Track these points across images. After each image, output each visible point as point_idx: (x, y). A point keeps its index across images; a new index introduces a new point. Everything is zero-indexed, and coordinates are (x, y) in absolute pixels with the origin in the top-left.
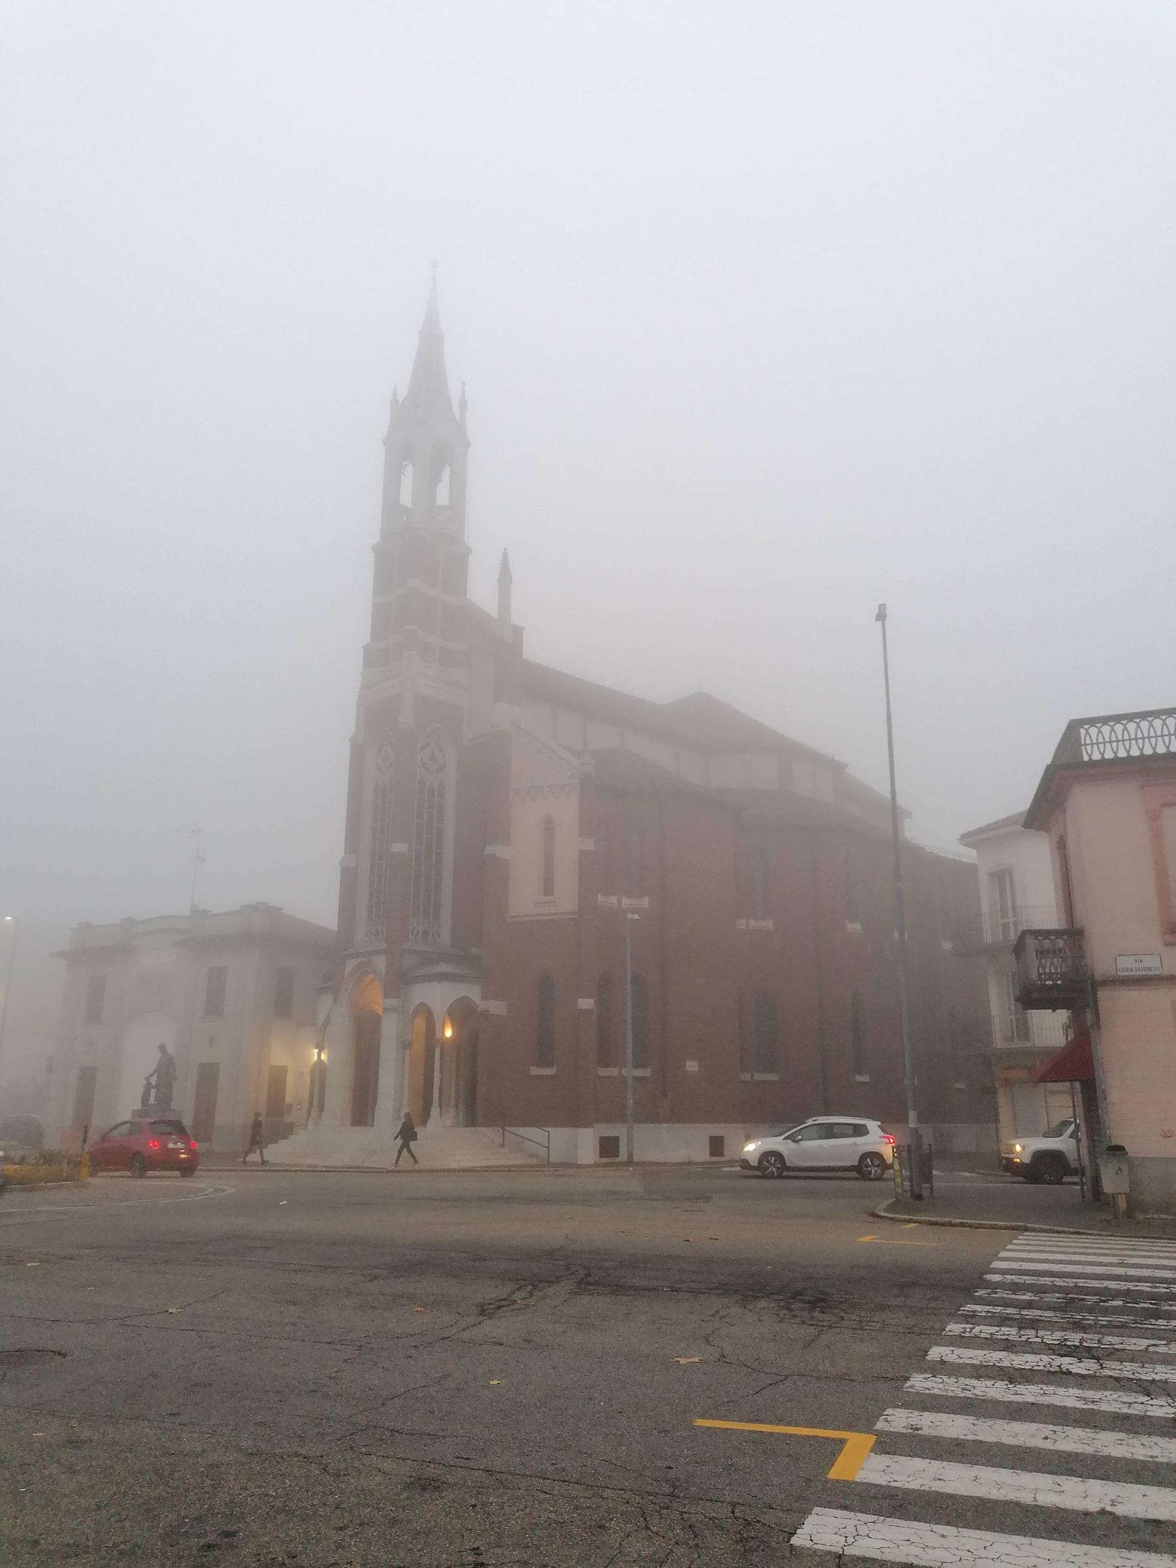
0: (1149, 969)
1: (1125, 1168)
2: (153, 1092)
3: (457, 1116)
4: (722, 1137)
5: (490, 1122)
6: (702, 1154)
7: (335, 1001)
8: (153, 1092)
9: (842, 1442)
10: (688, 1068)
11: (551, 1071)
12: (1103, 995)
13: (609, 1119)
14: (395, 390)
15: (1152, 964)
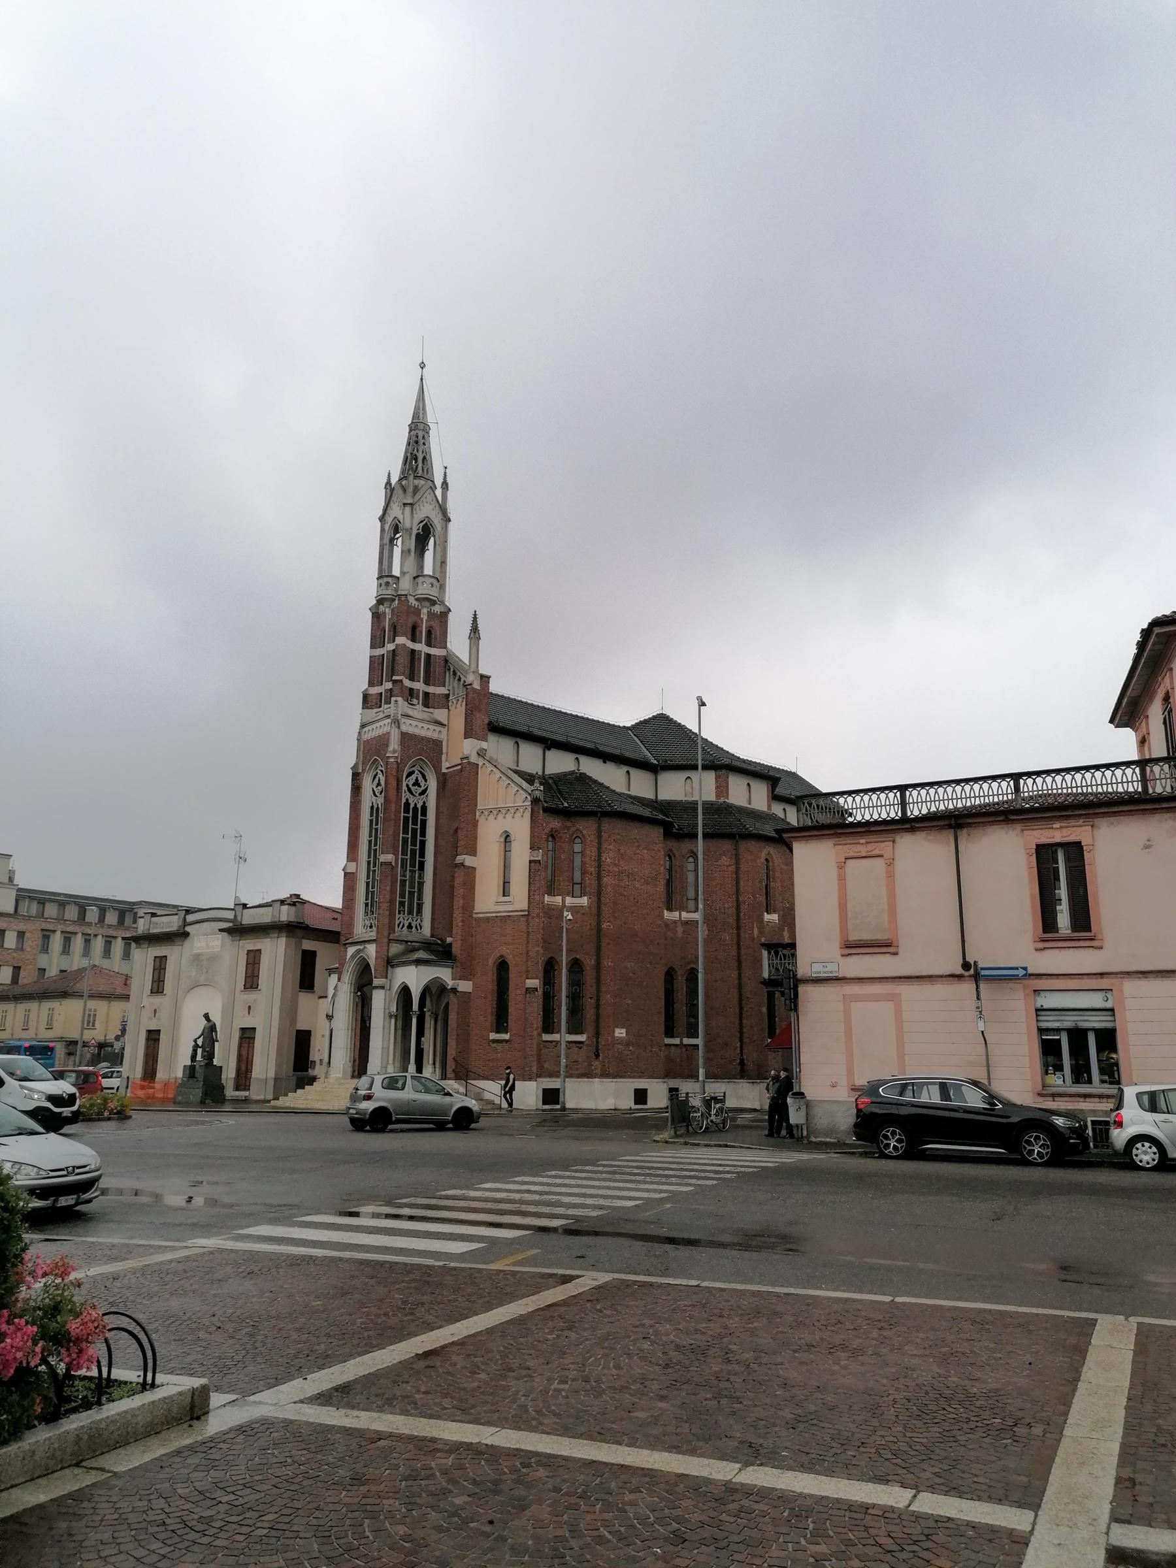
1: (803, 1108)
2: (200, 1051)
4: (646, 1090)
6: (628, 1103)
8: (200, 1051)
10: (617, 1035)
11: (507, 1037)
12: (802, 989)
13: (641, 1075)
14: (416, 458)
15: (831, 969)
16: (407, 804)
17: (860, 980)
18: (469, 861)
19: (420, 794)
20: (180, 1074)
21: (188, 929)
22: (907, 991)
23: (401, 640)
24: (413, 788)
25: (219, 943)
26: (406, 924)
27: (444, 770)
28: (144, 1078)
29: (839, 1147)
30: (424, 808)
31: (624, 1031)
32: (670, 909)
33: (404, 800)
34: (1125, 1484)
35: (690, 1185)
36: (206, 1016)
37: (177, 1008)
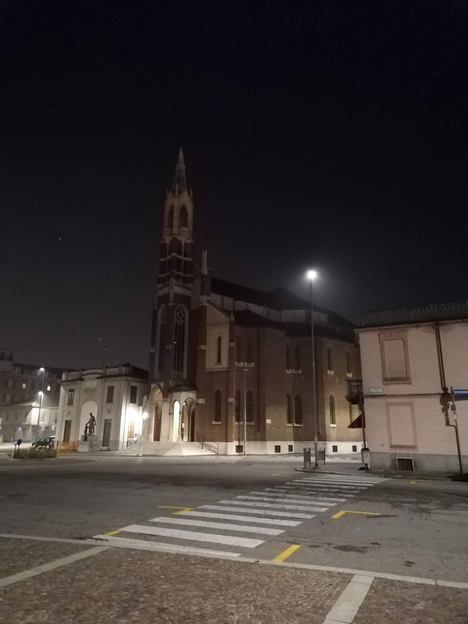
0: (379, 393)
2: (88, 429)
3: (188, 438)
5: (199, 440)
7: (148, 399)
8: (88, 429)
9: (352, 575)
13: (277, 440)
15: (380, 391)
16: (176, 323)
17: (393, 396)
18: (203, 347)
19: (182, 319)
20: (80, 439)
21: (83, 377)
22: (416, 401)
23: (173, 254)
24: (179, 317)
25: (96, 383)
26: (176, 375)
27: (192, 309)
28: (64, 441)
29: (386, 474)
30: (184, 325)
31: (270, 420)
32: (288, 368)
33: (175, 322)
34: (108, 400)
35: (335, 502)
36: (91, 414)
37: (79, 411)
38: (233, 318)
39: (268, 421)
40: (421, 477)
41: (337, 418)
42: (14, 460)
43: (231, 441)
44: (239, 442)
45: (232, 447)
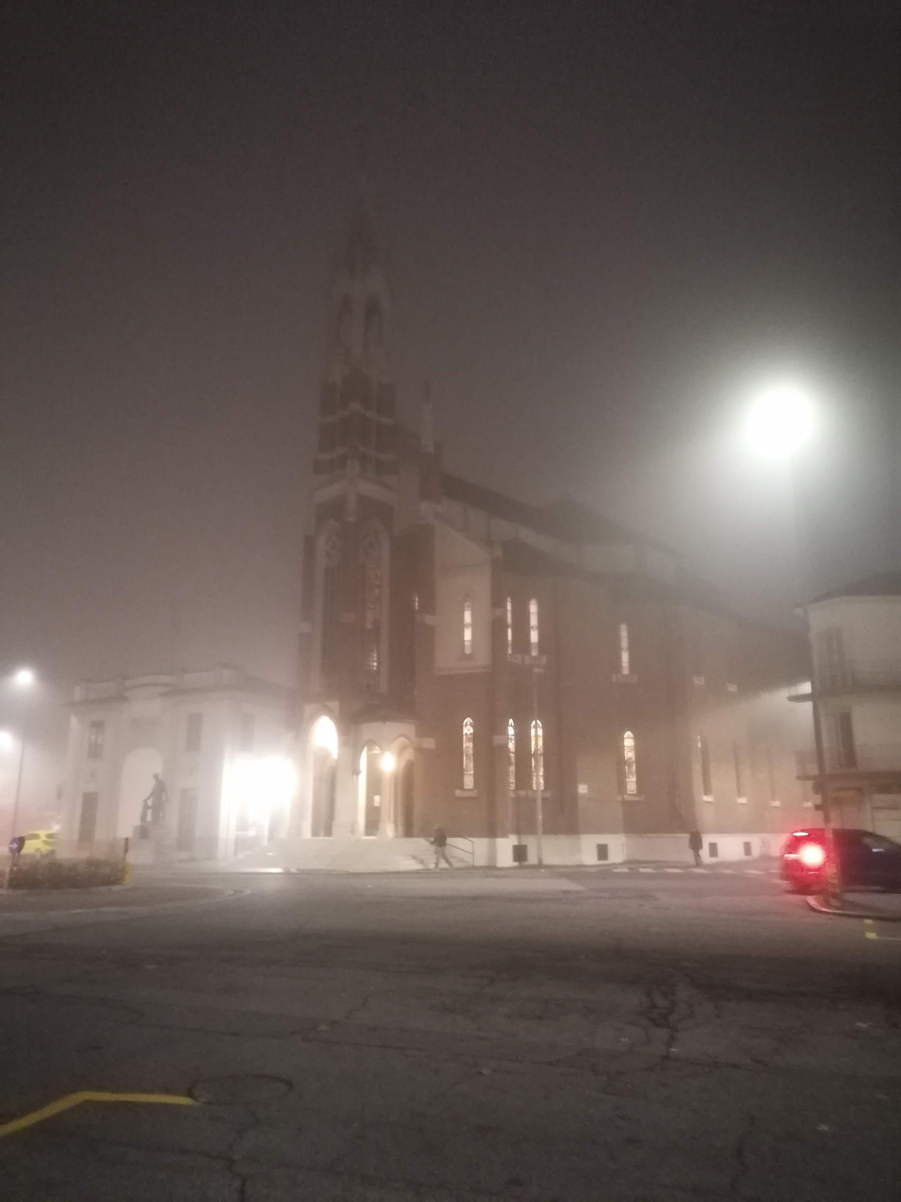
2: (150, 812)
8: (150, 812)
23: (355, 406)
38: (499, 553)
39: (583, 789)
40: (869, 914)
41: (714, 783)
42: (11, 892)
43: (504, 835)
44: (519, 839)
45: (505, 847)
